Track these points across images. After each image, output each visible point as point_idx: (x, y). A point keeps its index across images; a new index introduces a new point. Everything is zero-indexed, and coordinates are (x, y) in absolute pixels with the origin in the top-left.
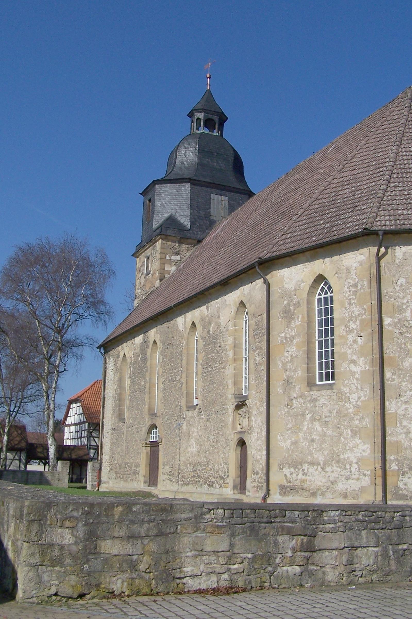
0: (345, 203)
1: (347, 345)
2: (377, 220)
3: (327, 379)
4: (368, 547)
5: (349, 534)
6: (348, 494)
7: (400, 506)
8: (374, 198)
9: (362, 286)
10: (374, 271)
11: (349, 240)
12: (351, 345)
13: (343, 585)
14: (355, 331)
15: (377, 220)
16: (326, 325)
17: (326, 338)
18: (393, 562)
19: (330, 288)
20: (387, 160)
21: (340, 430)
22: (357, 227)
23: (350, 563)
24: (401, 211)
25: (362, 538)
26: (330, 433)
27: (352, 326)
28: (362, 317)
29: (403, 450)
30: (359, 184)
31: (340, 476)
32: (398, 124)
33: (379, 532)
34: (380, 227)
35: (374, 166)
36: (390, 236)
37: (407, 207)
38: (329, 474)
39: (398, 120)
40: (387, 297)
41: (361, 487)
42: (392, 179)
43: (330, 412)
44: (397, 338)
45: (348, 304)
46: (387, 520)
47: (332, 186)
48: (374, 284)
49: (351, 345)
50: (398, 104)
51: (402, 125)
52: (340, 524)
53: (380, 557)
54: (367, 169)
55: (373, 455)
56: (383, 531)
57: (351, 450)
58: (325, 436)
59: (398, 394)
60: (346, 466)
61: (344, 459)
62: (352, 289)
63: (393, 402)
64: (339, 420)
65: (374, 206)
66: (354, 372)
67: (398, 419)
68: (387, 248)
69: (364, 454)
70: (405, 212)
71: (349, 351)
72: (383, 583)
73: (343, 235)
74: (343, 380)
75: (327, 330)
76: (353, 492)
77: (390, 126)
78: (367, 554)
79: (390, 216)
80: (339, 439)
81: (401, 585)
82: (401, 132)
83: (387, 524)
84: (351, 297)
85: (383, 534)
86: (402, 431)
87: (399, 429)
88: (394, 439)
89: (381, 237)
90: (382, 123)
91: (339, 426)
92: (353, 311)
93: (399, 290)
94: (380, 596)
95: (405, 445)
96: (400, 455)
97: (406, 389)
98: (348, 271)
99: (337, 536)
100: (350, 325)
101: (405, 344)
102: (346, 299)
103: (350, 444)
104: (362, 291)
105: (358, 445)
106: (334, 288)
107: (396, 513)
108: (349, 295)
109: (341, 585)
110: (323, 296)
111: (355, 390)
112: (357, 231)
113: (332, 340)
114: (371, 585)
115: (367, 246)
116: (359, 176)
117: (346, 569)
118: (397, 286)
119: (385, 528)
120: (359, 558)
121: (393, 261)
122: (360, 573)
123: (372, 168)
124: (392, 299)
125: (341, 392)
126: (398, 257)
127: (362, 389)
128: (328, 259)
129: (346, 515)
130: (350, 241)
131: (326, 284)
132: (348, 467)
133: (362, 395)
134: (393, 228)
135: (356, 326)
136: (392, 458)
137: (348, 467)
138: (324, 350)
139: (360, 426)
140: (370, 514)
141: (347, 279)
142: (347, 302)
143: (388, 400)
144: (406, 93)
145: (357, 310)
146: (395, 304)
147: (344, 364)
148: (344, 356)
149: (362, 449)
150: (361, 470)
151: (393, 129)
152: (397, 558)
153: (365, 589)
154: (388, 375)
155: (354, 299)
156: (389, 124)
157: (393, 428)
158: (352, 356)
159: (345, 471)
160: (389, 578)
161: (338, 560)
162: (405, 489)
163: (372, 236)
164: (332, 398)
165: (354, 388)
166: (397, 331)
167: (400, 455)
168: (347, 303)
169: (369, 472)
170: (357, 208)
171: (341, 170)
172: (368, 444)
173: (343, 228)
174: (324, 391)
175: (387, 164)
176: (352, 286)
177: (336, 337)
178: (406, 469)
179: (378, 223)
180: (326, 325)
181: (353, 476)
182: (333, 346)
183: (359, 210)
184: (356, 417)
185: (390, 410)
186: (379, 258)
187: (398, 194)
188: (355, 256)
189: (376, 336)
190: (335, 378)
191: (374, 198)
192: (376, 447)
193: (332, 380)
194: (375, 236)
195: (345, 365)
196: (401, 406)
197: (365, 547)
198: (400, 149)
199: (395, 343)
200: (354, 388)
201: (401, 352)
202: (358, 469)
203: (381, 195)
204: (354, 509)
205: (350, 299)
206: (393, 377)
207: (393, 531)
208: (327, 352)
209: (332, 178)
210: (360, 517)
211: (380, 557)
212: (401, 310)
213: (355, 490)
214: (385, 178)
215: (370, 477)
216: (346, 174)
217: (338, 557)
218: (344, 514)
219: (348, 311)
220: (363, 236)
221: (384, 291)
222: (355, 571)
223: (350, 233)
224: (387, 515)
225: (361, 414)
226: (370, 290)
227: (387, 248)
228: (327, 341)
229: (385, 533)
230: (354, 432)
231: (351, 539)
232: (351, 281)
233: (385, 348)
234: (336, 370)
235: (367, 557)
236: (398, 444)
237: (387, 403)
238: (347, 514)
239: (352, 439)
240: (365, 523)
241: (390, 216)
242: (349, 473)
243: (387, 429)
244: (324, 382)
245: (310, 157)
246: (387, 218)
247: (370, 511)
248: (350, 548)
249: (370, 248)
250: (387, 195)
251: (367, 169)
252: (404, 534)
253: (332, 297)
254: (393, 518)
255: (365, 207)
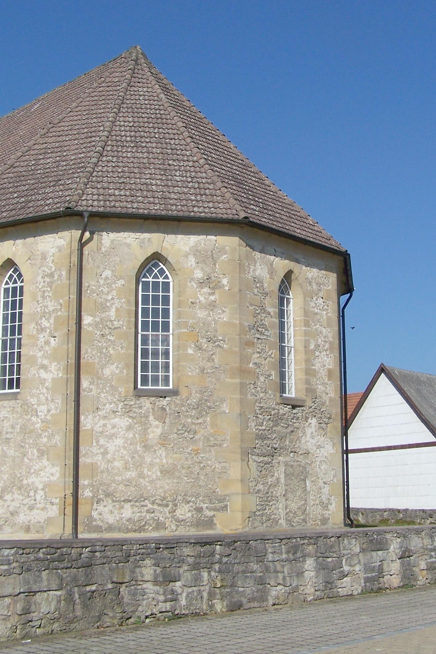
0: (47, 174)
1: (37, 346)
2: (83, 198)
3: (11, 387)
4: (50, 591)
5: (26, 576)
6: (31, 527)
7: (89, 540)
8: (82, 172)
9: (60, 276)
10: (75, 259)
11: (49, 219)
12: (42, 347)
13: (17, 639)
14: (48, 331)
15: (83, 198)
16: (13, 321)
17: (11, 337)
18: (78, 607)
19: (20, 276)
20: (102, 128)
21: (24, 450)
22: (58, 205)
23: (26, 611)
24: (112, 191)
25: (41, 581)
26: (11, 452)
27: (45, 323)
28: (57, 313)
29: (99, 474)
30: (65, 154)
31: (22, 506)
32: (118, 88)
33: (63, 572)
34: (85, 208)
35: (85, 135)
36: (97, 219)
37: (120, 186)
38: (8, 503)
39: (118, 83)
40: (89, 292)
41: (48, 518)
42: (105, 152)
43: (13, 427)
44: (98, 341)
45: (41, 297)
46: (74, 558)
47: (32, 152)
48: (74, 275)
49: (42, 347)
50: (121, 64)
51: (123, 89)
52: (15, 564)
53: (63, 602)
54: (77, 136)
55: (63, 479)
56: (68, 571)
57: (37, 473)
58: (6, 457)
59: (95, 407)
60: (29, 493)
61: (28, 484)
62: (47, 279)
63: (89, 417)
64: (24, 436)
65: (81, 181)
66: (45, 379)
67: (94, 437)
68: (92, 233)
69: (52, 478)
70: (117, 193)
71: (40, 354)
72: (66, 632)
73: (40, 214)
74: (30, 389)
75: (13, 328)
76: (37, 524)
77: (108, 89)
78: (47, 599)
79: (99, 195)
80: (22, 460)
81: (86, 634)
82: (120, 98)
83: (73, 563)
84: (46, 289)
85: (67, 574)
86: (98, 451)
87: (95, 448)
88: (89, 460)
89: (86, 219)
90: (99, 84)
91: (23, 444)
92: (47, 306)
93: (104, 284)
94: (60, 648)
95: (102, 468)
96: (95, 479)
97: (105, 401)
98: (44, 257)
99: (11, 580)
100: (41, 323)
101: (107, 349)
102: (40, 291)
103: (35, 466)
104: (59, 282)
105: (45, 467)
106: (25, 277)
107: (84, 549)
108: (43, 287)
109: (13, 640)
110: (11, 285)
111: (44, 401)
112: (58, 210)
113: (19, 340)
114: (50, 637)
115: (68, 228)
116: (66, 144)
117: (20, 620)
118: (102, 278)
119: (71, 567)
120: (37, 606)
121: (99, 249)
122: (38, 623)
123: (83, 136)
124: (95, 294)
125: (27, 404)
126: (105, 245)
127: (52, 401)
128: (21, 241)
129: (23, 554)
130: (48, 221)
131: (16, 270)
132: (32, 494)
133: (53, 407)
134: (101, 209)
135: (49, 324)
136: (86, 482)
137: (32, 494)
138: (8, 351)
139: (48, 445)
140: (53, 551)
141: (42, 266)
142: (40, 294)
143: (83, 414)
144: (130, 53)
145: (51, 305)
146: (97, 300)
147: (32, 369)
148: (33, 360)
149: (51, 473)
150: (47, 498)
151: (111, 93)
152: (84, 602)
153: (43, 642)
154: (84, 384)
155: (49, 292)
156: (108, 87)
157: (88, 448)
158: (42, 361)
159: (28, 499)
160: (73, 626)
161: (11, 609)
162: (100, 519)
163: (75, 217)
164: (16, 410)
165: (43, 398)
166: (98, 333)
167: (95, 479)
168: (40, 296)
169: (57, 501)
170: (60, 182)
171: (45, 135)
172: (57, 466)
173: (42, 205)
174: (7, 402)
175: (101, 134)
176: (47, 276)
177: (24, 336)
178: (101, 496)
179: (84, 203)
180: (13, 321)
181: (38, 505)
182: (20, 347)
183: (63, 185)
184: (44, 434)
185: (85, 426)
186: (82, 245)
187: (110, 170)
188: (53, 239)
189: (73, 338)
190: (21, 386)
191: (82, 172)
192: (67, 469)
193: (16, 389)
194: (78, 218)
195: (33, 371)
196: (98, 422)
197: (45, 591)
198: (118, 118)
199: (95, 347)
200: (43, 398)
201: (101, 358)
202: (44, 496)
203: (90, 169)
204: (33, 546)
205: (44, 291)
206: (91, 387)
207: (80, 570)
208: (12, 354)
209: (32, 142)
210: (41, 555)
211: (63, 602)
212: (104, 308)
213: (39, 522)
214: (97, 150)
215: (58, 506)
216: (50, 140)
217: (11, 605)
218: (21, 552)
219: (41, 305)
220: (65, 216)
221: (85, 284)
222: (31, 621)
223: (49, 212)
224: (73, 552)
225: (50, 431)
226: (68, 282)
227: (92, 233)
228: (12, 340)
229: (70, 573)
230: (41, 452)
231: (28, 583)
232: (47, 270)
233: (83, 352)
234: (22, 377)
235: (47, 603)
236: (93, 467)
237: (82, 418)
238: (25, 551)
239: (38, 461)
240: (47, 562)
241: (99, 195)
242: (33, 502)
243: (81, 448)
244: (7, 391)
245: (9, 115)
246: (95, 197)
247: (53, 548)
248: (26, 594)
249: (72, 231)
250: (98, 170)
251: (77, 136)
252: (92, 573)
253: (22, 288)
254: (81, 554)
255: (70, 182)
